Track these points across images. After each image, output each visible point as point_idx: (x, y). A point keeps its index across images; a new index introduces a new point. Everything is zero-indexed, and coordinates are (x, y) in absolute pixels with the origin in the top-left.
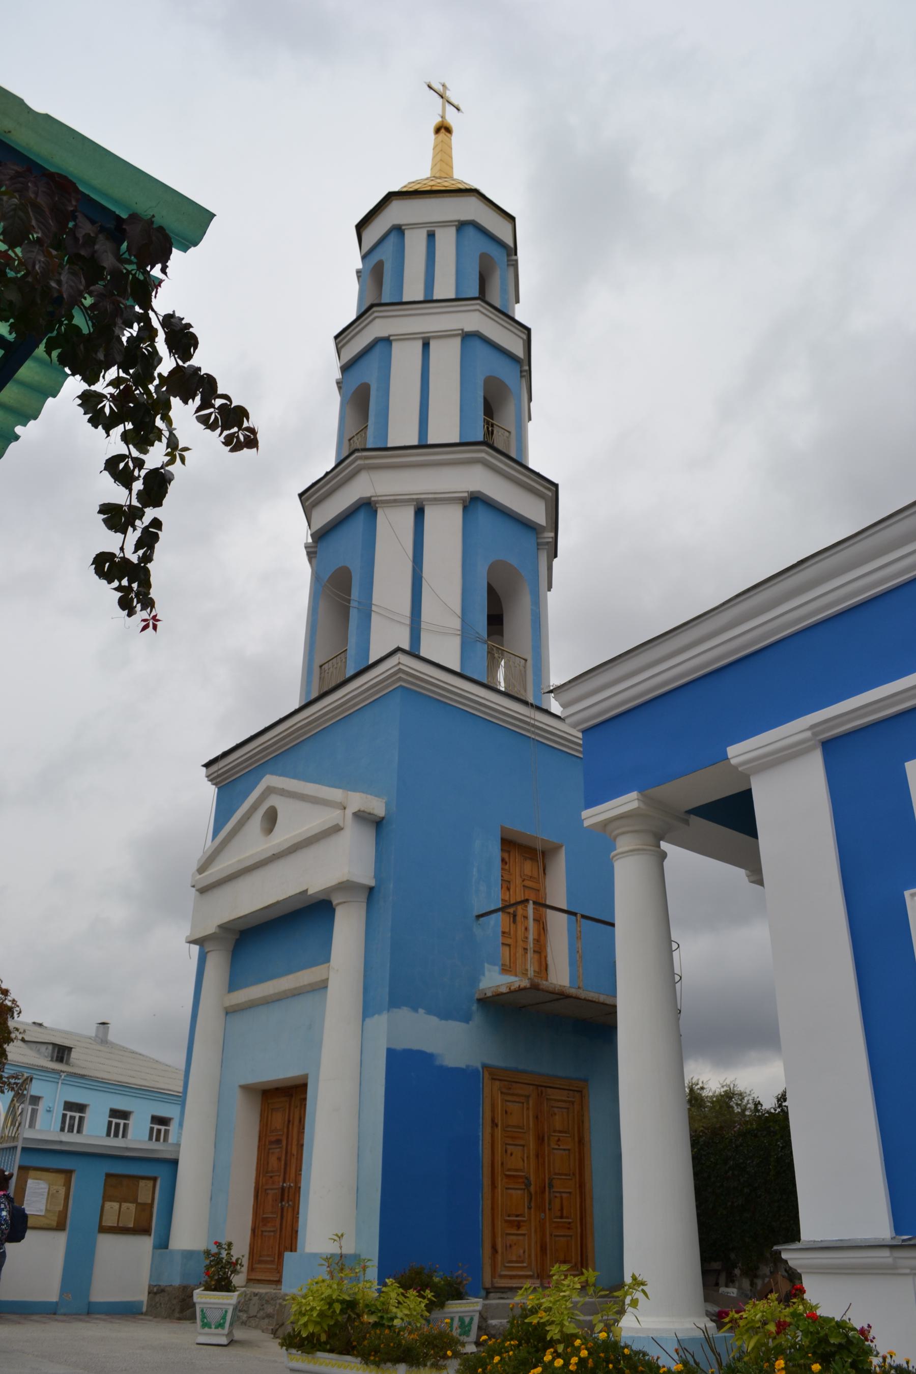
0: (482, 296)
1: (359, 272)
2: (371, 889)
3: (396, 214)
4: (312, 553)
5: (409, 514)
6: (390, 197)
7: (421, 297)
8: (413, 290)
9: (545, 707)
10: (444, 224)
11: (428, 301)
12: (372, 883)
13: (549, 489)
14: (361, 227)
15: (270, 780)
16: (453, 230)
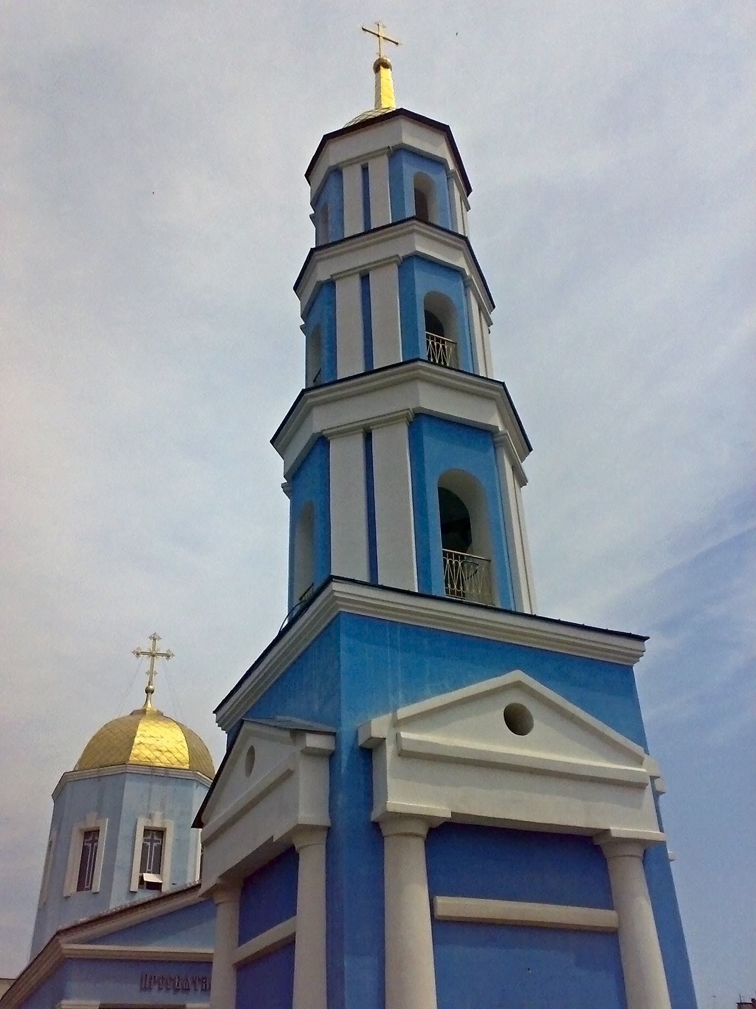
0: (422, 216)
1: (312, 217)
2: (329, 829)
3: (337, 154)
4: (289, 489)
5: (358, 441)
6: (327, 138)
7: (361, 230)
8: (353, 225)
9: (519, 611)
10: (374, 155)
11: (368, 231)
12: (326, 822)
13: (497, 390)
14: (308, 175)
15: (518, 675)
16: (385, 159)
